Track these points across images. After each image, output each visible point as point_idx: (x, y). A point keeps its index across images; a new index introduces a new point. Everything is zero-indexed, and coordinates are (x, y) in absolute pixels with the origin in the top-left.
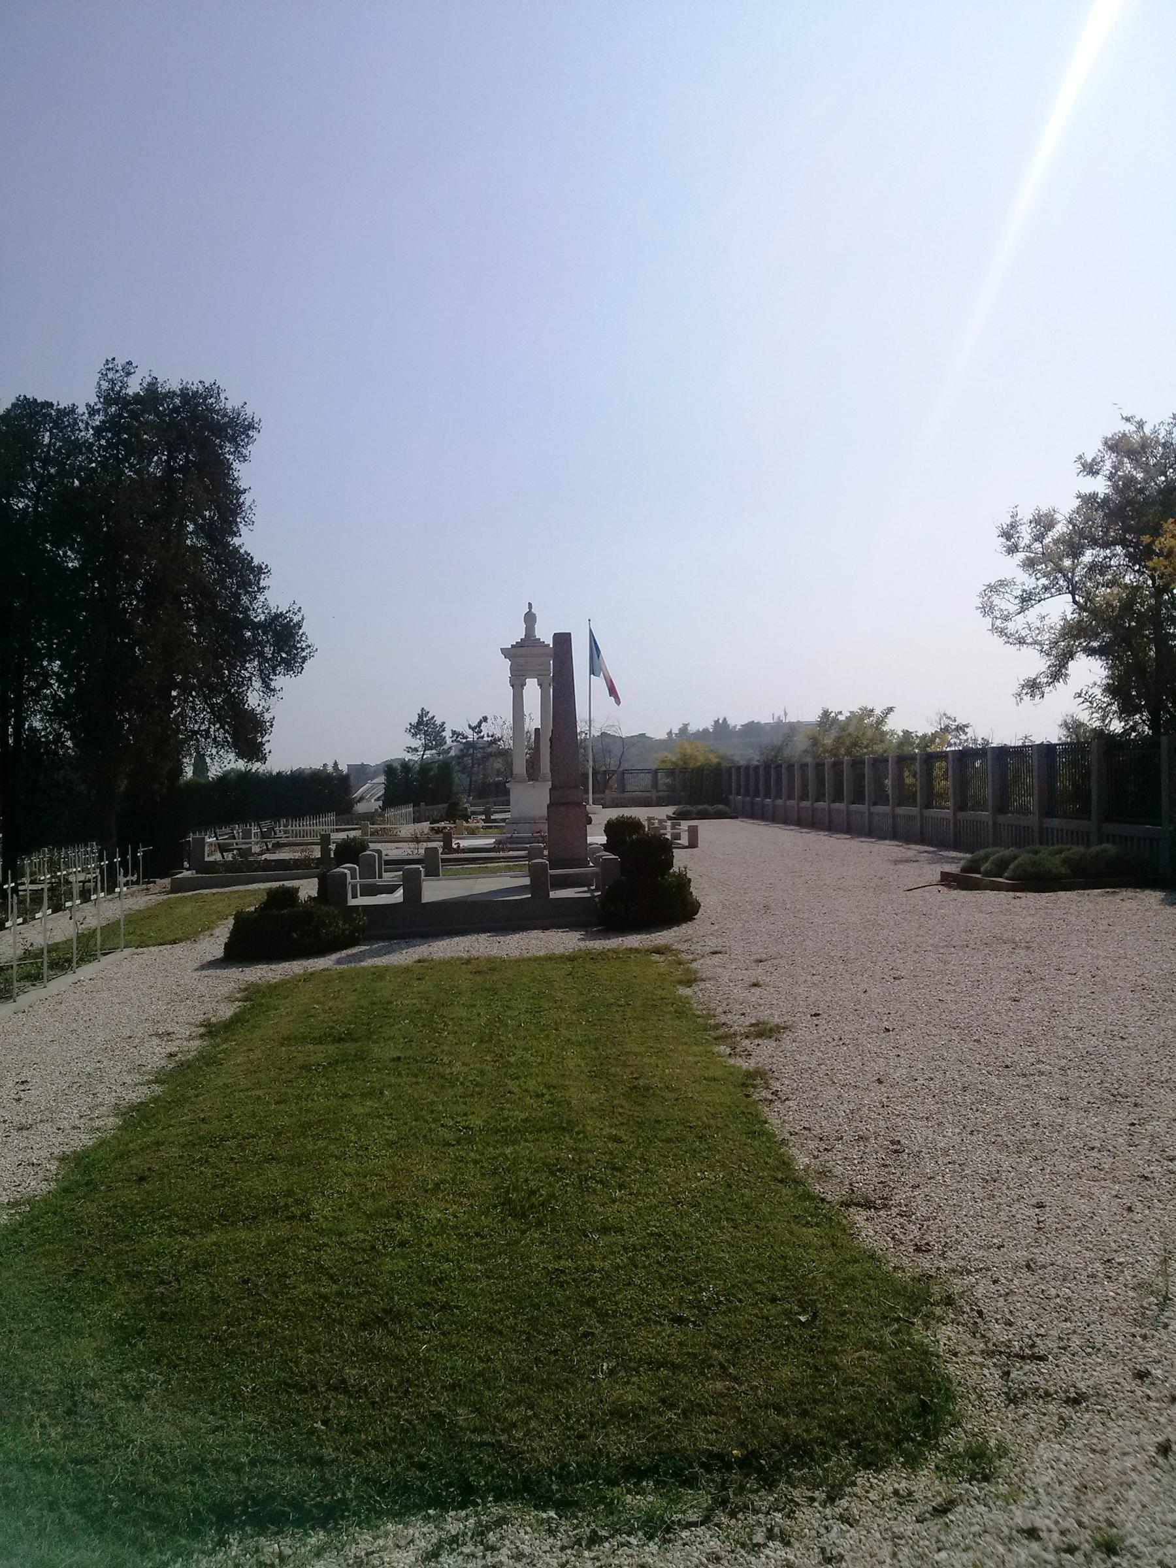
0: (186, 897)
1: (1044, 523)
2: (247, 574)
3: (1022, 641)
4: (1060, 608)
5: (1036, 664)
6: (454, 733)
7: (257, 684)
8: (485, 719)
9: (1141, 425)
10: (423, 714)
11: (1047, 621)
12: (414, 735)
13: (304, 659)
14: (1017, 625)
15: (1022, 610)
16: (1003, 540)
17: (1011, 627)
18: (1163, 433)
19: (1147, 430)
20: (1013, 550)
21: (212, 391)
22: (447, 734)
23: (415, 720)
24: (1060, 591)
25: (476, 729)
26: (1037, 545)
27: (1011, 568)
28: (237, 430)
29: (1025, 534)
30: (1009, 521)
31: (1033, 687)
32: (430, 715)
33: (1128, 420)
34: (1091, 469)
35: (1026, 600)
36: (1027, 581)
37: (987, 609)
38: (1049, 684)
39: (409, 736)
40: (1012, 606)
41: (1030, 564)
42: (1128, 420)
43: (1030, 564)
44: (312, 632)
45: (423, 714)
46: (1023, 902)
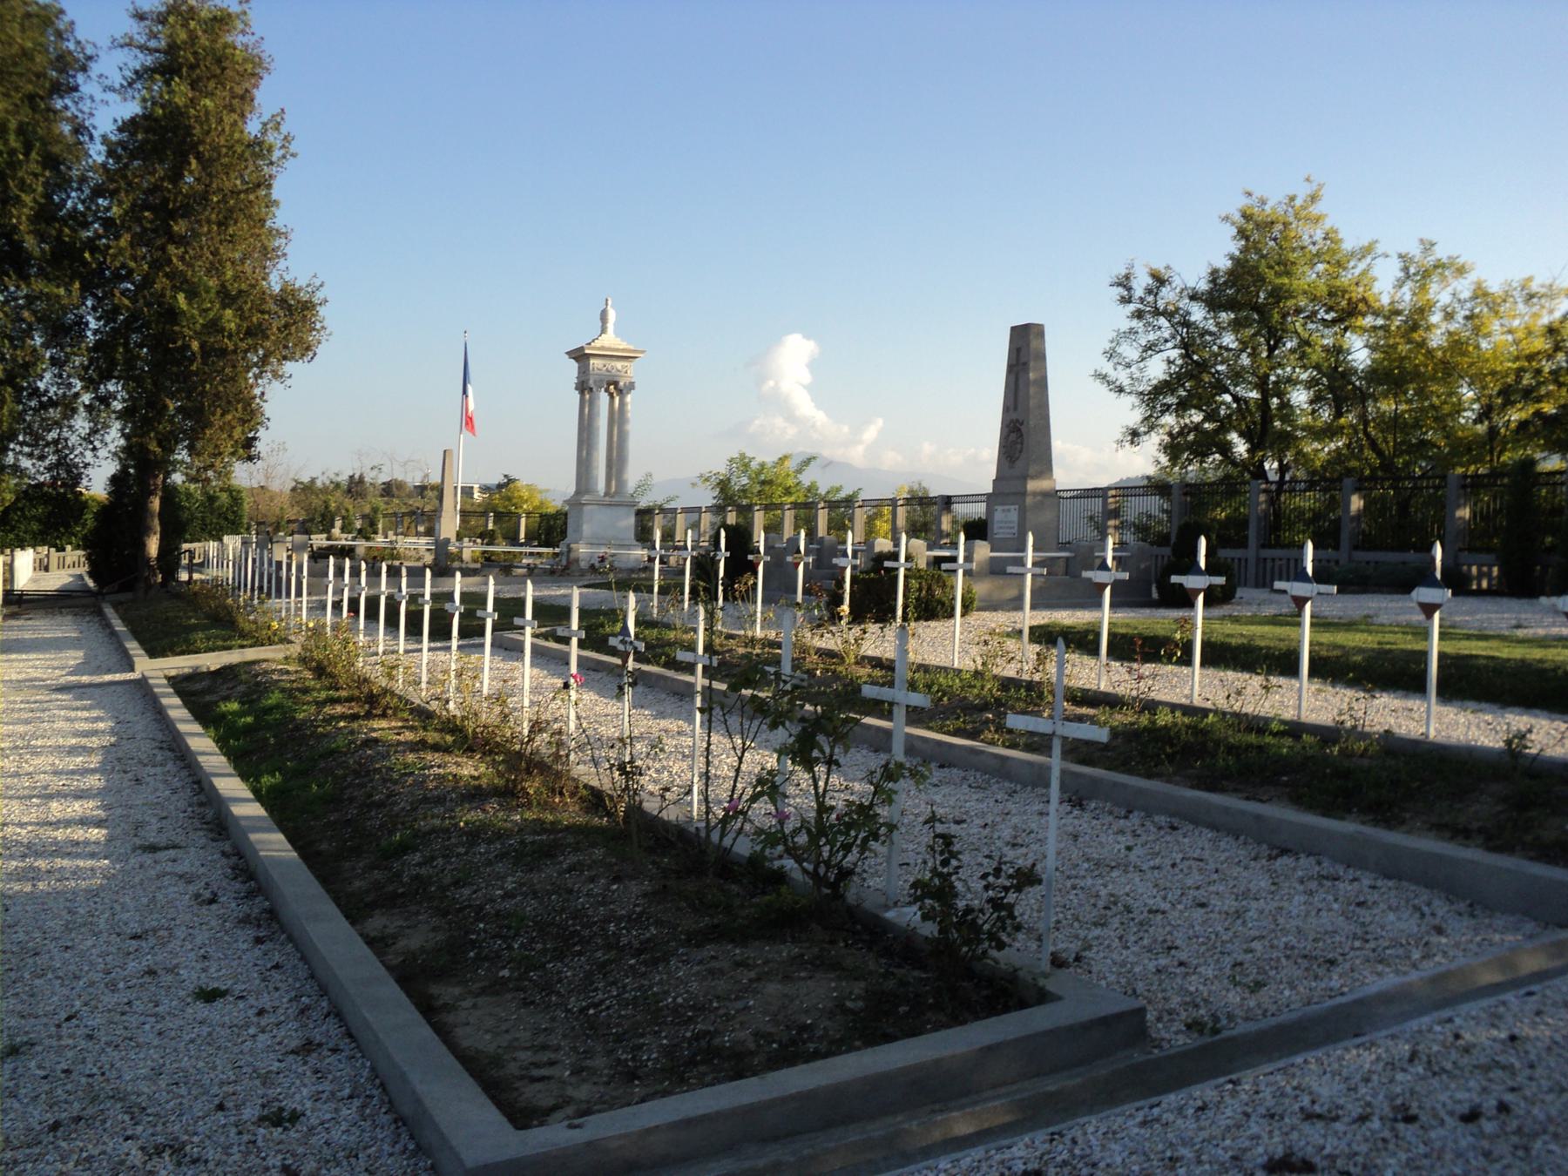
3: (1121, 390)
9: (1263, 202)
14: (1122, 377)
19: (1268, 208)
20: (1125, 300)
27: (1121, 318)
29: (1141, 283)
30: (1124, 272)
41: (1139, 315)
43: (1139, 315)
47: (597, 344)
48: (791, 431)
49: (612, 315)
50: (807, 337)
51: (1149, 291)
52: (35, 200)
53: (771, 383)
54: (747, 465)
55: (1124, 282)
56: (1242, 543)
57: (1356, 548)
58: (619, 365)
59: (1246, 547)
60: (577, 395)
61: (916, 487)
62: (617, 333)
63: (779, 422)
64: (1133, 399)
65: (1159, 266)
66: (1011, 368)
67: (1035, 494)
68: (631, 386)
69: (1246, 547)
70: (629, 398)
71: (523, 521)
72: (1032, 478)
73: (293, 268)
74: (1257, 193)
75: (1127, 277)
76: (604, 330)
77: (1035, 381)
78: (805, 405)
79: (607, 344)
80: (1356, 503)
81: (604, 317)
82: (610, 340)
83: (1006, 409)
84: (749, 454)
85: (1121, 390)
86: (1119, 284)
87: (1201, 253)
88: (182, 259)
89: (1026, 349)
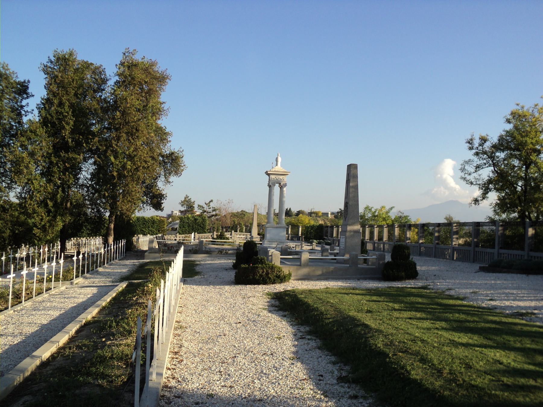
0: (153, 259)
1: (484, 140)
2: (162, 135)
3: (472, 183)
4: (487, 173)
5: (477, 193)
6: (199, 206)
7: (162, 178)
8: (212, 201)
9: (523, 107)
10: (187, 197)
11: (481, 177)
12: (182, 205)
13: (183, 170)
14: (471, 178)
15: (476, 171)
16: (468, 144)
17: (468, 177)
18: (531, 111)
19: (525, 109)
20: (471, 149)
21: (153, 64)
22: (196, 206)
23: (183, 200)
24: (490, 166)
25: (208, 204)
26: (480, 148)
27: (470, 155)
28: (162, 79)
29: (476, 142)
30: (470, 137)
31: (476, 201)
32: (189, 198)
33: (518, 105)
34: (508, 121)
35: (478, 167)
36: (477, 161)
37: (463, 170)
38: (481, 200)
39: (180, 206)
40: (473, 170)
41: (477, 154)
42: (518, 105)
43: (477, 154)
44: (186, 160)
45: (187, 197)
46: (279, 325)
47: (273, 170)
48: (447, 193)
49: (280, 159)
50: (453, 160)
51: (480, 145)
52: (71, 128)
53: (439, 176)
54: (370, 210)
55: (470, 142)
56: (493, 247)
57: (531, 250)
58: (281, 177)
59: (494, 248)
60: (268, 188)
61: (448, 217)
62: (281, 166)
63: (442, 188)
64: (477, 187)
65: (484, 134)
66: (347, 181)
67: (350, 231)
68: (285, 185)
69: (494, 248)
70: (285, 189)
71: (300, 229)
72: (350, 225)
73: (173, 145)
74: (521, 105)
75: (471, 140)
76: (277, 165)
77: (353, 187)
78: (452, 183)
79: (276, 170)
80: (531, 231)
81: (277, 160)
82: (279, 168)
83: (345, 198)
84: (370, 206)
85: (472, 183)
86: (469, 143)
87: (496, 129)
88: (117, 145)
89: (352, 172)
